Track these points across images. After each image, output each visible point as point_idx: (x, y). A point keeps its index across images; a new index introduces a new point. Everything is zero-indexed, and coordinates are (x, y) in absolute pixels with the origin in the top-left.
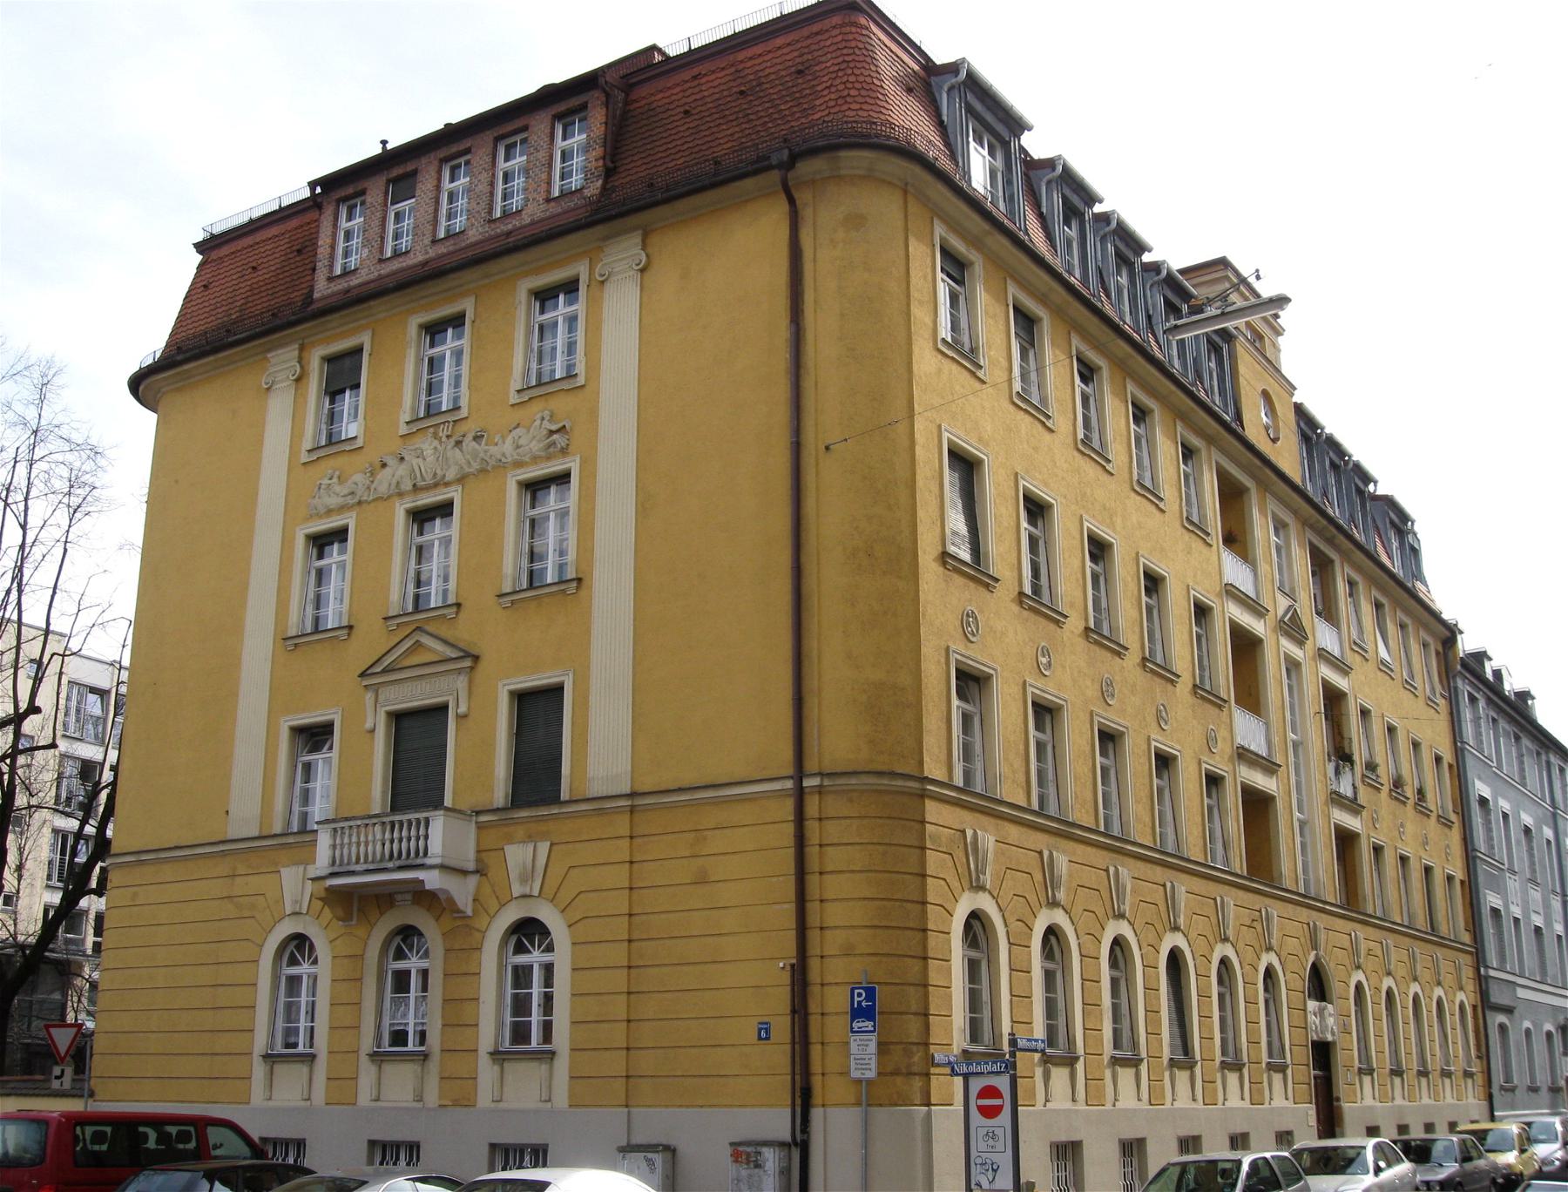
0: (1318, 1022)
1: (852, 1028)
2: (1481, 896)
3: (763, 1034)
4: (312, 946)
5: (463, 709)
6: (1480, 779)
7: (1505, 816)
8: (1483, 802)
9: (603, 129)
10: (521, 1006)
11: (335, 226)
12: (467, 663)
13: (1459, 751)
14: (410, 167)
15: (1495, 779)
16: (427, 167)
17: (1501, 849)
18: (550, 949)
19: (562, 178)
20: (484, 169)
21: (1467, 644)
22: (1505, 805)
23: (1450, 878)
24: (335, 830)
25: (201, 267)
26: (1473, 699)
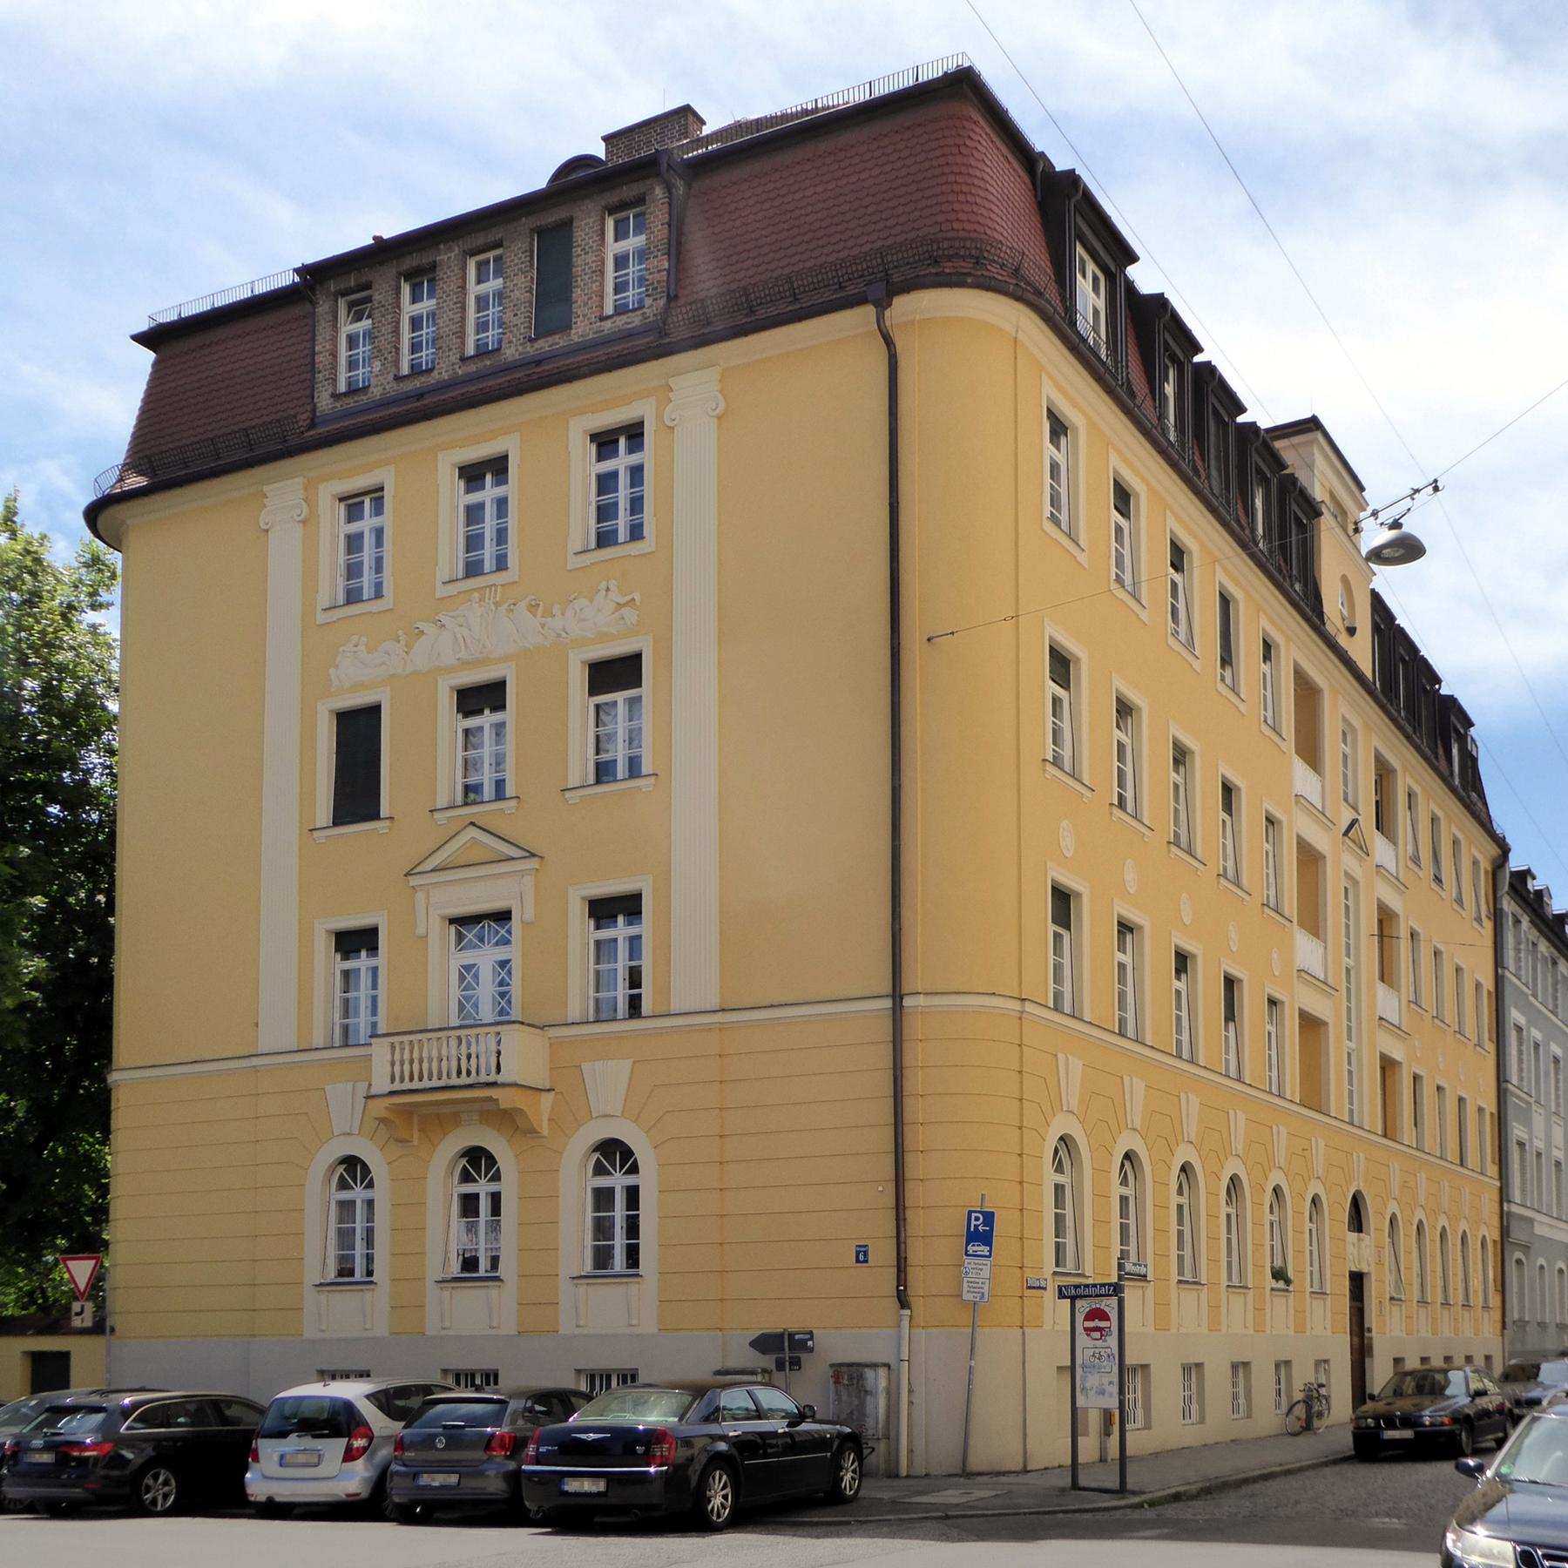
0: (1355, 1253)
1: (966, 1251)
2: (1509, 1129)
3: (861, 1257)
4: (366, 1170)
5: (529, 916)
6: (1516, 1007)
7: (1537, 1046)
8: (1519, 1029)
9: (666, 231)
10: (345, 1238)
11: (335, 327)
12: (533, 863)
13: (1499, 981)
14: (425, 259)
15: (1528, 1009)
16: (448, 256)
17: (1530, 1082)
18: (497, 1177)
19: (616, 292)
20: (520, 269)
21: (1516, 863)
22: (1536, 1034)
23: (1481, 1110)
24: (393, 1046)
25: (155, 365)
26: (1517, 922)
